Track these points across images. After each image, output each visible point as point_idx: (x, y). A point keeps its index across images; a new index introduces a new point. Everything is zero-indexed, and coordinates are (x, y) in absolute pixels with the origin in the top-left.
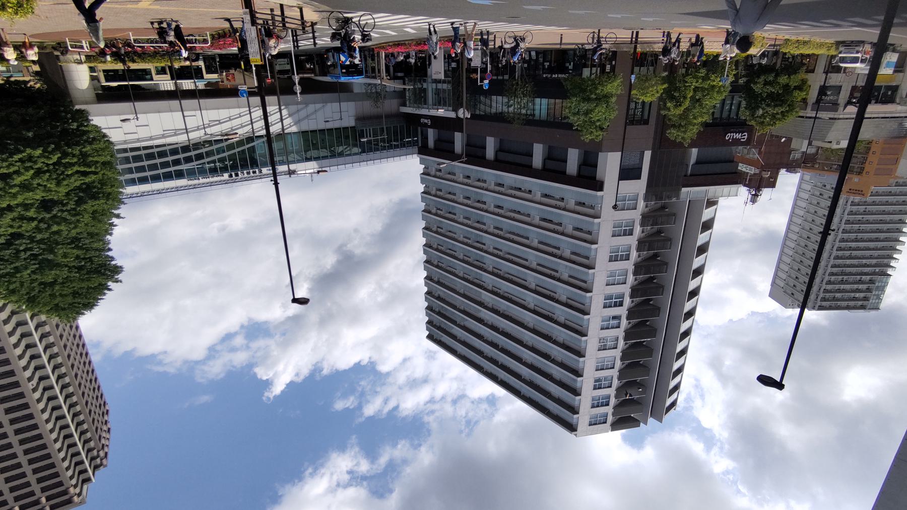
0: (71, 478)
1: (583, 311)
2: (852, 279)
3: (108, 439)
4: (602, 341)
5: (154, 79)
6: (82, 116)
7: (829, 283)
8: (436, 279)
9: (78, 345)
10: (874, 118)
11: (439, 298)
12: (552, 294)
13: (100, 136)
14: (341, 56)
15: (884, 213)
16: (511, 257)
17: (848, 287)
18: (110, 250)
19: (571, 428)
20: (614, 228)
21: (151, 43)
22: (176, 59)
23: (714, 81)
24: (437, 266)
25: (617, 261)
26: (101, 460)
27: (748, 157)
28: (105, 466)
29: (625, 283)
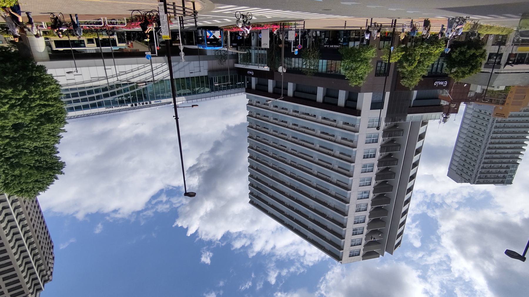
0: (30, 288)
1: (347, 188)
2: (496, 166)
3: (53, 264)
4: (358, 206)
5: (86, 46)
6: (42, 69)
7: (483, 168)
8: (255, 168)
9: (35, 207)
10: (521, 73)
11: (257, 179)
12: (328, 178)
13: (51, 80)
14: (207, 32)
15: (515, 127)
16: (302, 155)
17: (494, 170)
18: (58, 152)
19: (339, 258)
20: (366, 138)
21: (87, 24)
22: (100, 34)
23: (432, 50)
24: (256, 160)
25: (368, 158)
26: (48, 277)
27: (442, 95)
28: (51, 280)
29: (372, 171)
